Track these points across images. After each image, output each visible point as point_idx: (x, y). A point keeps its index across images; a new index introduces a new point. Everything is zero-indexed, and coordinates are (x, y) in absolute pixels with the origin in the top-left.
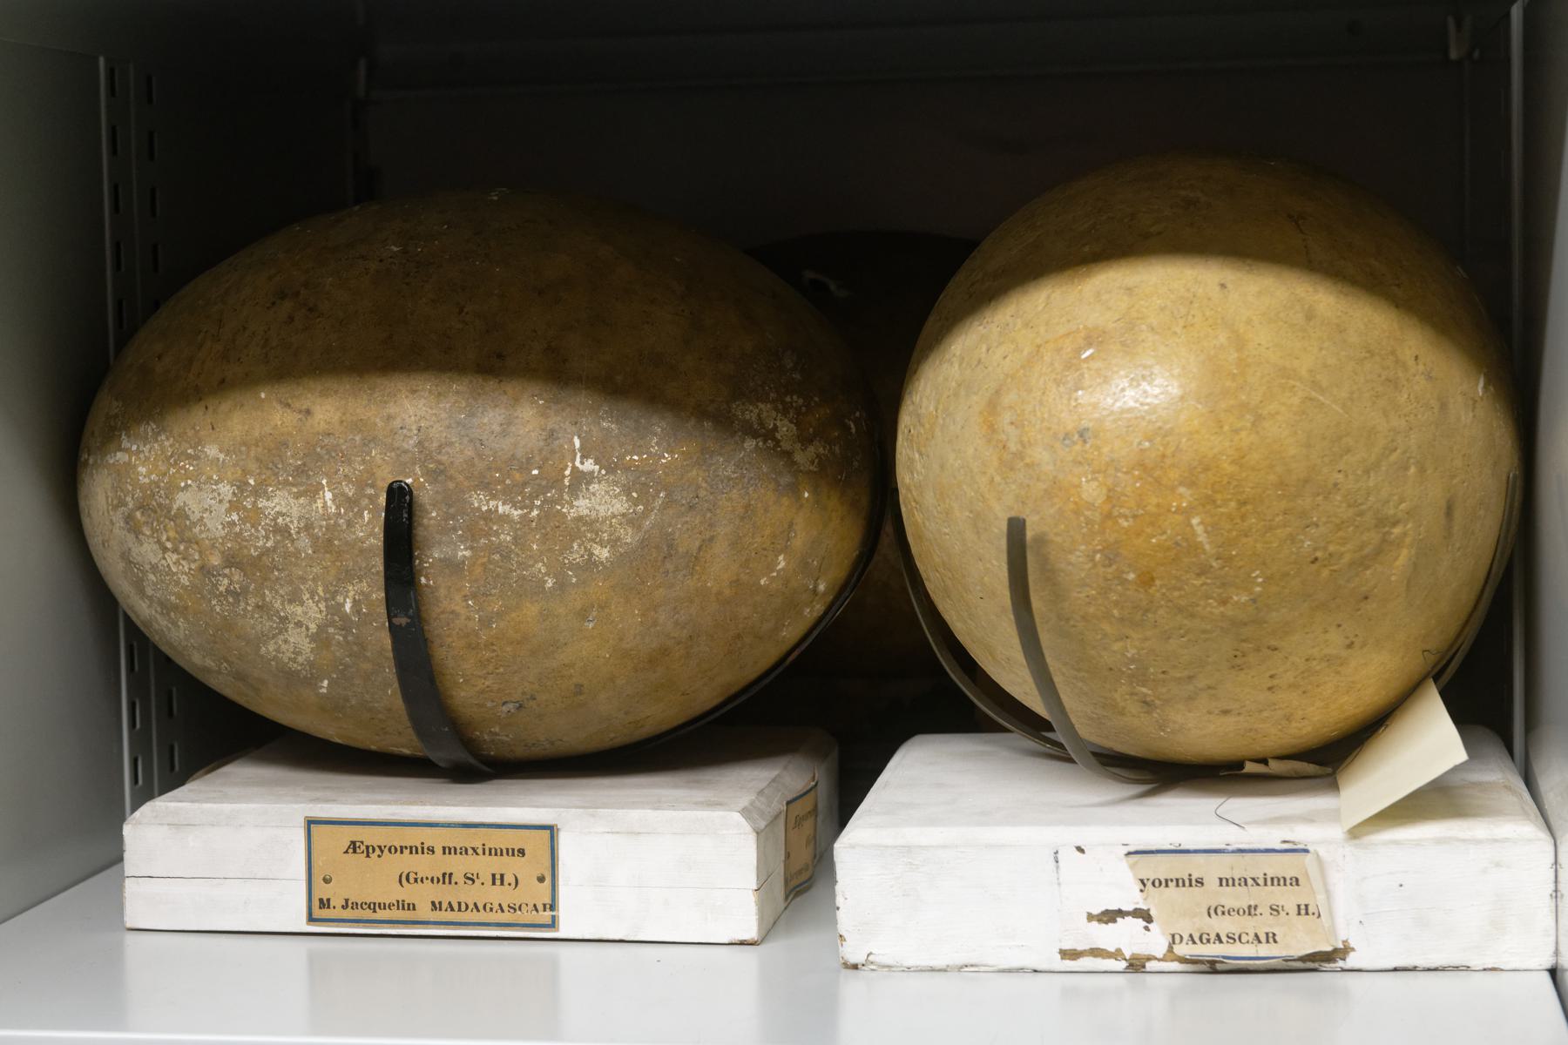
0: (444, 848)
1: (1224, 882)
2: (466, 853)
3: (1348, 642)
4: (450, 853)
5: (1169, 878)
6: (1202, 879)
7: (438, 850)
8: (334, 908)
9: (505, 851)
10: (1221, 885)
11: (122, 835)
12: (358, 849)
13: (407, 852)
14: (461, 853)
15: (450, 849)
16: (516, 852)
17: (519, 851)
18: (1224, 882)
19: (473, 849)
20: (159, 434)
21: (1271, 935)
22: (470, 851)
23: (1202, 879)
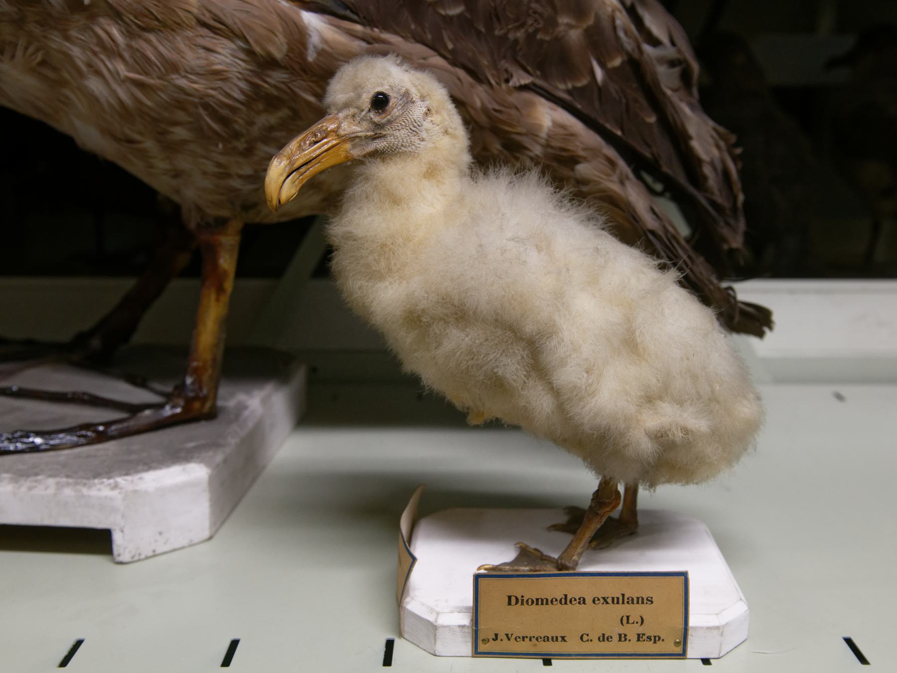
0: (620, 635)
1: (513, 600)
2: (613, 599)
3: (445, 297)
4: (542, 604)
5: (532, 636)
6: (652, 598)
7: (589, 600)
8: (630, 640)
9: (635, 601)
10: (510, 604)
11: (599, 487)
12: (641, 639)
13: (527, 640)
14: (628, 603)
15: (542, 600)
16: (645, 601)
17: (651, 640)
18: (513, 600)
19: (607, 603)
20: (466, 327)
21: (623, 636)
22: (609, 600)
23: (652, 598)
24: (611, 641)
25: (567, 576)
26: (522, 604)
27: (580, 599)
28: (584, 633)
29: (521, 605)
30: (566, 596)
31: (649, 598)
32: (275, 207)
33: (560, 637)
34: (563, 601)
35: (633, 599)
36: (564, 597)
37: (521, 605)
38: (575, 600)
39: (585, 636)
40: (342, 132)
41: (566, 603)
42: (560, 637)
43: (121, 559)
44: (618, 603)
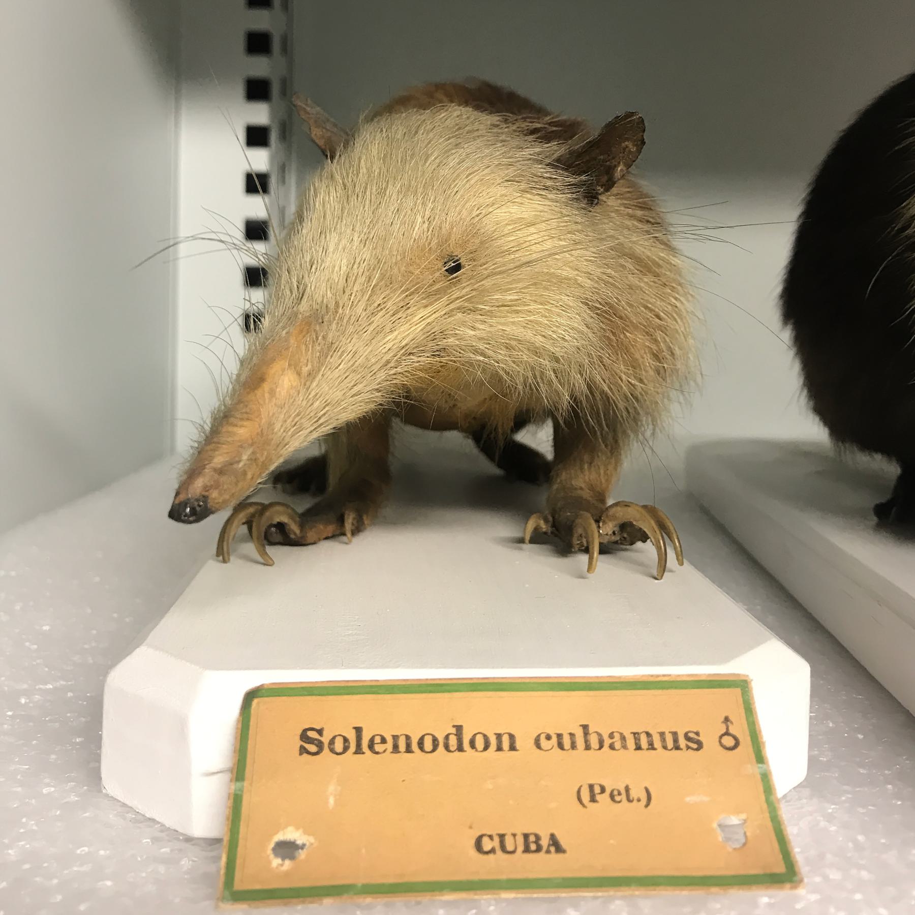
7: (525, 742)
23: (303, 750)
24: (619, 802)
25: (561, 690)
26: (359, 751)
27: (611, 736)
28: (484, 832)
29: (356, 753)
30: (459, 729)
31: (691, 735)
32: (593, 469)
33: (681, 749)
34: (453, 741)
35: (623, 738)
36: (454, 731)
37: (356, 753)
38: (384, 741)
39: (485, 840)
40: (607, 155)
41: (460, 748)
42: (681, 749)
43: (644, 733)
44: (573, 746)
